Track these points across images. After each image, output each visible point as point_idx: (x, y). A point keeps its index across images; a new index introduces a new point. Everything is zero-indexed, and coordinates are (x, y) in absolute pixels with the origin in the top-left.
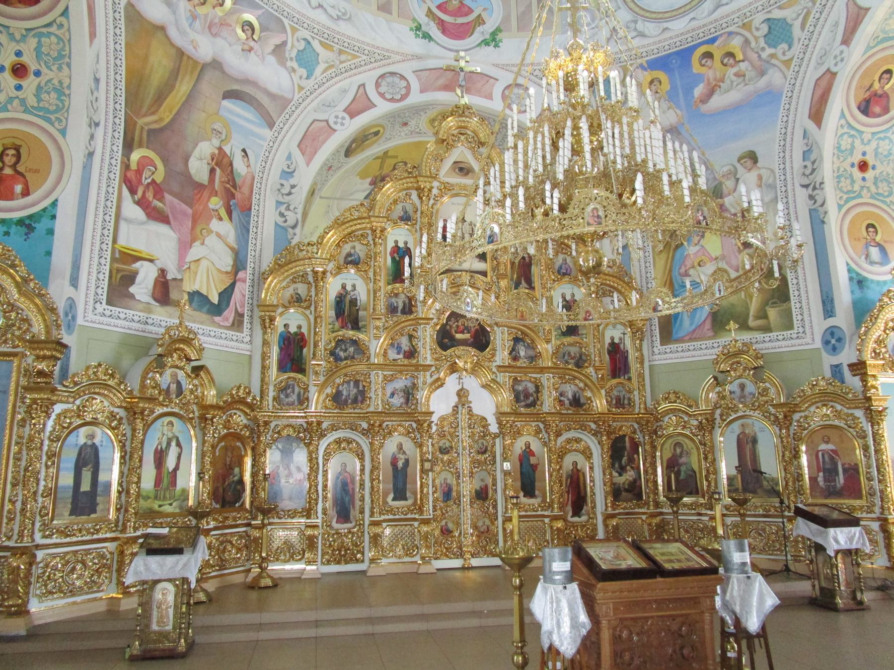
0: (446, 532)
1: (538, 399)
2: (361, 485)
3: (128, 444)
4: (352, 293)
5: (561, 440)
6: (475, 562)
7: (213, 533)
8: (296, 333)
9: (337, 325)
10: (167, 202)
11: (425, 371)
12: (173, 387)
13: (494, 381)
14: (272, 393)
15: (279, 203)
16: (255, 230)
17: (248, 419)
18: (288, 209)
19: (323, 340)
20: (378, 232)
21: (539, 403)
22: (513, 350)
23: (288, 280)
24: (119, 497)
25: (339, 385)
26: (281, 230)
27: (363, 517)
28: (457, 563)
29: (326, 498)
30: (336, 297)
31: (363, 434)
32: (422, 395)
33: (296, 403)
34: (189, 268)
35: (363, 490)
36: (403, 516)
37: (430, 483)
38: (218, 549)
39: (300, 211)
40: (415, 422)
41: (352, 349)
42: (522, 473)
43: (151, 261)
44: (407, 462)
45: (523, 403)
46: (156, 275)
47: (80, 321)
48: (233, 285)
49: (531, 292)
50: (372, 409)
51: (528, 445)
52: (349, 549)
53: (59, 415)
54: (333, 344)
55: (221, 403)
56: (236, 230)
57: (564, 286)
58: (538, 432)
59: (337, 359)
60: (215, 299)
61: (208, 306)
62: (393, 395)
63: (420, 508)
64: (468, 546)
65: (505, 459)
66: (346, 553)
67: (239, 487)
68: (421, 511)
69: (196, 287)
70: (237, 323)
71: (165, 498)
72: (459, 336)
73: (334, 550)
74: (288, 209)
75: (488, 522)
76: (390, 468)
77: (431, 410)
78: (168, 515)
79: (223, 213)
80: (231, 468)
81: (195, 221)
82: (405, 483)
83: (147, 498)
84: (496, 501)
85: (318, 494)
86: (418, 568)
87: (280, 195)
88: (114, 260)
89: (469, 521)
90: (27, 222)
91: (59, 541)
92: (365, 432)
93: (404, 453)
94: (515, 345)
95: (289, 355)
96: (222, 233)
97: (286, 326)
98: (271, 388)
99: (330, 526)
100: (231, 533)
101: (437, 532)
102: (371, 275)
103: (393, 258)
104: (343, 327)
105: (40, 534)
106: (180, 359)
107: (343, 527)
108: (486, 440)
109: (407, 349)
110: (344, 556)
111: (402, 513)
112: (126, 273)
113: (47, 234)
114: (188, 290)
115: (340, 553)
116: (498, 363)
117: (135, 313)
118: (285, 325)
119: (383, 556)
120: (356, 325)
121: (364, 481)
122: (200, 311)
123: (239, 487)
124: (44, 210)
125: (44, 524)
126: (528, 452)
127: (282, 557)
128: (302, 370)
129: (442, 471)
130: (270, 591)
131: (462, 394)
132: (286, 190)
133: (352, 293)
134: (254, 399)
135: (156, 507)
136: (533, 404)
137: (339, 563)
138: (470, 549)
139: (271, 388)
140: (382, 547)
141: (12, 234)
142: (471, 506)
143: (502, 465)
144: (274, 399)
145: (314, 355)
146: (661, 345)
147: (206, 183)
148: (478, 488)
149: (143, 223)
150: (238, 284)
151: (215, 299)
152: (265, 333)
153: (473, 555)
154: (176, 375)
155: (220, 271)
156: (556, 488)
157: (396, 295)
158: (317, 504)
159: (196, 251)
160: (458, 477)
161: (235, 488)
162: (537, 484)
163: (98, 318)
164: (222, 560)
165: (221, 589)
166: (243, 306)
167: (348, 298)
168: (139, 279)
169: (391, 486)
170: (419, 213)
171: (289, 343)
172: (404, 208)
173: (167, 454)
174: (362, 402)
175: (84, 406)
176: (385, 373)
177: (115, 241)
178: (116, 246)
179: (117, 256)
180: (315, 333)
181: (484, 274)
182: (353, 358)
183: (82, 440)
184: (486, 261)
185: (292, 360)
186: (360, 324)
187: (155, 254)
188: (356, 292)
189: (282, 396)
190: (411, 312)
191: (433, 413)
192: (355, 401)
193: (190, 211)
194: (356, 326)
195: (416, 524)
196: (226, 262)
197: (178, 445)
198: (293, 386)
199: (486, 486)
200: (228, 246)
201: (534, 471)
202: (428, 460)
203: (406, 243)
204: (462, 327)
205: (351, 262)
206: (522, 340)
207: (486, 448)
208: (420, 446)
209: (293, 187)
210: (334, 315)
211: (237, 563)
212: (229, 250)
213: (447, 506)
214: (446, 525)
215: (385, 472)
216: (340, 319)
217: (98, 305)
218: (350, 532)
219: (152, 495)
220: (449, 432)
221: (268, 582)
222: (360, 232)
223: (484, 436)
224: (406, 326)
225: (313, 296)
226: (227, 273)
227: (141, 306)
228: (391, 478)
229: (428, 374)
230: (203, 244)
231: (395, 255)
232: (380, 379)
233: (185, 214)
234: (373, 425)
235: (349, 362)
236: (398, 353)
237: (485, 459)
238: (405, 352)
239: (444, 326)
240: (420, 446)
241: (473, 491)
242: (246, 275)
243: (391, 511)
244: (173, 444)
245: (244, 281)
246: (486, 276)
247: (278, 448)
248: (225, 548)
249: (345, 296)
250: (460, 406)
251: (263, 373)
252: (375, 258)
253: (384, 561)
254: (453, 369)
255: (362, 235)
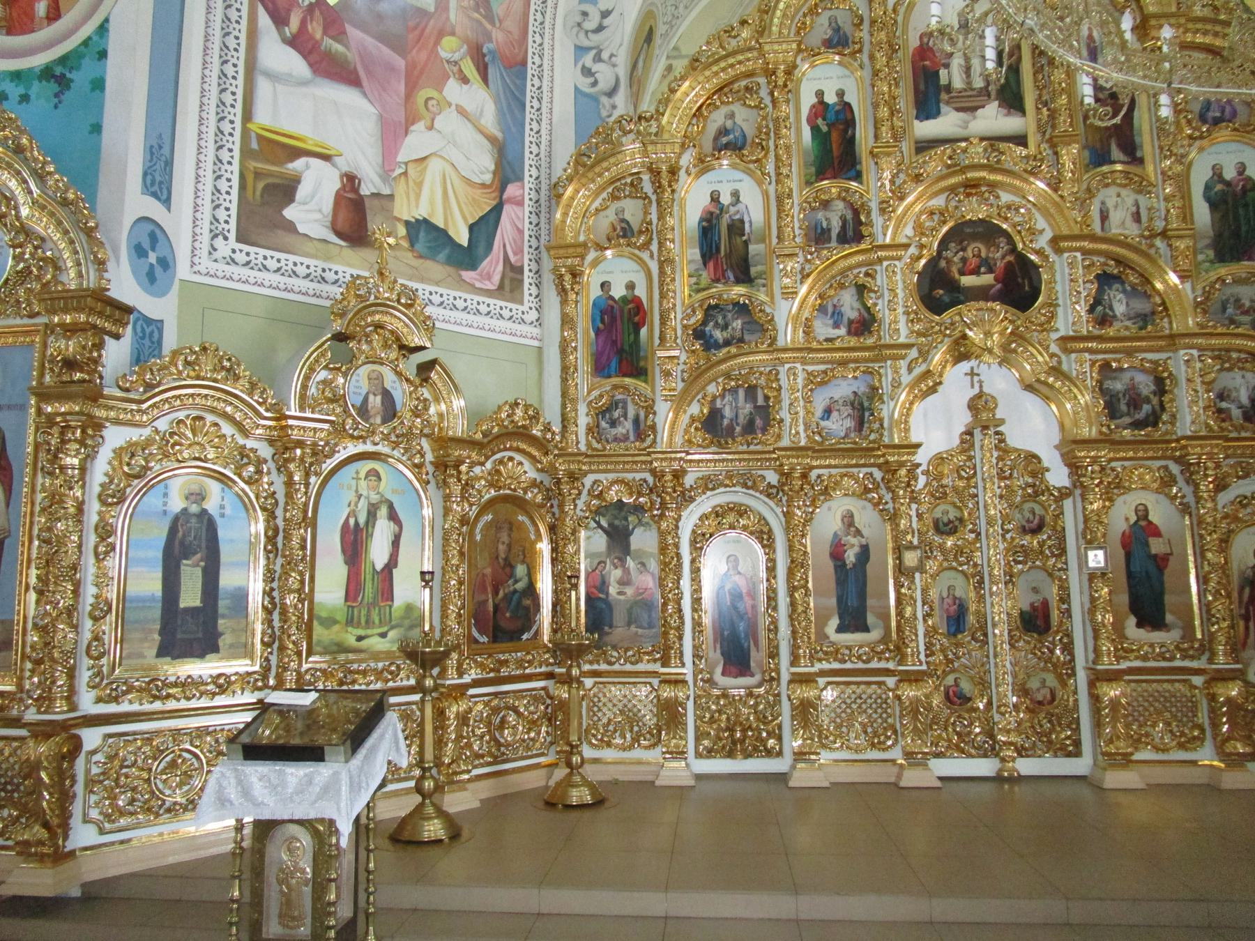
0: (956, 699)
1: (1163, 408)
2: (769, 598)
3: (279, 512)
4: (732, 209)
5: (1225, 498)
6: (1026, 766)
7: (472, 691)
8: (624, 298)
9: (705, 277)
10: (353, 44)
11: (896, 358)
12: (376, 402)
13: (1056, 371)
14: (583, 420)
15: (580, 50)
16: (536, 104)
17: (538, 470)
18: (597, 58)
19: (679, 309)
20: (780, 74)
21: (1165, 417)
22: (1097, 301)
23: (604, 195)
24: (269, 622)
25: (714, 398)
26: (585, 101)
27: (777, 665)
28: (984, 767)
29: (700, 624)
30: (701, 220)
31: (768, 496)
32: (890, 410)
33: (632, 438)
34: (405, 174)
35: (775, 609)
36: (860, 665)
37: (918, 595)
38: (490, 723)
39: (623, 61)
40: (879, 466)
41: (738, 324)
42: (1130, 575)
43: (326, 158)
44: (865, 553)
45: (1127, 420)
46: (338, 185)
47: (183, 270)
48: (497, 210)
49: (1131, 168)
50: (785, 442)
51: (1143, 513)
52: (750, 728)
53: (118, 452)
54: (699, 315)
55: (479, 436)
56: (497, 101)
57: (1221, 148)
58: (1167, 481)
59: (710, 344)
60: (463, 238)
61: (447, 251)
62: (828, 412)
63: (898, 648)
64: (1008, 732)
65: (1091, 543)
66: (745, 737)
67: (527, 602)
68: (899, 652)
69: (421, 212)
70: (510, 285)
71: (369, 624)
72: (967, 281)
73: (719, 729)
74: (597, 58)
75: (1051, 680)
76: (829, 566)
77: (914, 439)
78: (376, 656)
79: (469, 69)
80: (509, 566)
81: (412, 87)
82: (862, 595)
83: (329, 622)
84: (1069, 635)
85: (681, 617)
86: (899, 776)
87: (582, 35)
88: (246, 153)
89: (1009, 679)
90: (58, 70)
91: (136, 707)
92: (770, 492)
93: (858, 533)
94: (1100, 291)
95: (614, 342)
96: (469, 108)
97: (605, 286)
98: (582, 409)
99: (710, 681)
100: (514, 692)
101: (936, 701)
102: (770, 167)
103: (815, 129)
104: (717, 280)
105: (93, 694)
106: (386, 346)
107: (737, 686)
108: (1041, 504)
109: (853, 315)
110: (742, 741)
111: (859, 658)
112: (270, 180)
113: (93, 90)
114: (405, 218)
115: (732, 736)
116: (1062, 333)
117: (298, 259)
118: (603, 285)
119: (824, 746)
120: (743, 272)
121: (775, 591)
122: (432, 258)
123: (527, 602)
124: (86, 43)
125: (99, 673)
126: (1143, 529)
127: (618, 741)
128: (639, 372)
129: (942, 570)
130: (587, 814)
131: (980, 405)
132: (591, 24)
133: (732, 209)
134: (547, 428)
135: (351, 640)
136: (1153, 420)
137: (731, 755)
138: (1013, 738)
139: (582, 409)
140: (819, 729)
141: (33, 97)
142: (1012, 646)
143: (1083, 560)
144: (589, 430)
145: (662, 338)
146: (522, 303)
147: (432, 9)
148: (1026, 607)
149: (304, 83)
150: (508, 210)
151: (463, 238)
152: (564, 302)
153: (1021, 752)
154: (380, 377)
155: (468, 182)
156: (1219, 608)
157: (826, 204)
158: (680, 638)
159: (416, 143)
160: (981, 582)
161: (519, 603)
162: (1169, 599)
163: (222, 266)
164: (499, 744)
165: (497, 806)
166: (519, 251)
167: (725, 220)
168: (302, 192)
169: (833, 601)
170: (866, 26)
171: (613, 320)
172: (833, 21)
173: (370, 536)
174: (764, 430)
175: (172, 434)
176: (810, 368)
177: (248, 116)
178: (249, 125)
179: (254, 145)
180: (663, 296)
181: (1021, 140)
182: (741, 340)
183: (177, 504)
184: (1022, 111)
185: (620, 352)
186: (753, 271)
187: (332, 142)
188: (740, 207)
189: (603, 424)
190: (859, 238)
191: (918, 446)
192: (749, 428)
193: (400, 63)
194: (744, 275)
195: (891, 681)
196: (482, 165)
197: (393, 516)
198: (625, 402)
199: (1045, 604)
200: (481, 132)
201: (1161, 570)
202: (911, 547)
203: (841, 94)
204: (974, 262)
205: (727, 146)
206: (1117, 278)
207: (1042, 519)
208: (894, 517)
209: (605, 14)
210: (698, 256)
211: (528, 748)
212: (486, 142)
213: (958, 645)
214: (957, 684)
215: (819, 572)
216: (711, 265)
217: (219, 242)
218: (750, 695)
219: (341, 617)
220: (955, 489)
221: (579, 795)
222: (743, 83)
223: (1036, 494)
224: (850, 268)
225: (655, 221)
226: (483, 186)
227: (309, 247)
228: (833, 584)
229: (903, 364)
230: (431, 128)
231: (820, 121)
232: (800, 380)
233: (392, 69)
234: (788, 475)
235: (734, 350)
236: (836, 325)
237: (1042, 544)
238: (851, 322)
239: (933, 263)
240: (894, 517)
241: (1015, 613)
242: (525, 189)
243: (835, 654)
244: (383, 511)
245: (520, 203)
246: (1025, 145)
247: (600, 526)
248: (503, 721)
249: (719, 217)
250: (977, 432)
251: (564, 380)
252: (777, 129)
253: (825, 757)
254: (961, 351)
255: (747, 89)
